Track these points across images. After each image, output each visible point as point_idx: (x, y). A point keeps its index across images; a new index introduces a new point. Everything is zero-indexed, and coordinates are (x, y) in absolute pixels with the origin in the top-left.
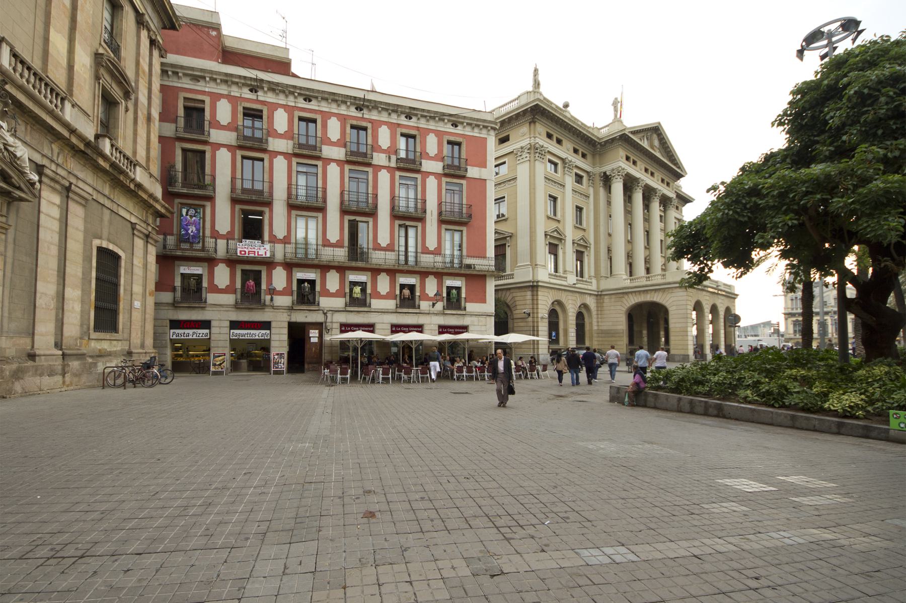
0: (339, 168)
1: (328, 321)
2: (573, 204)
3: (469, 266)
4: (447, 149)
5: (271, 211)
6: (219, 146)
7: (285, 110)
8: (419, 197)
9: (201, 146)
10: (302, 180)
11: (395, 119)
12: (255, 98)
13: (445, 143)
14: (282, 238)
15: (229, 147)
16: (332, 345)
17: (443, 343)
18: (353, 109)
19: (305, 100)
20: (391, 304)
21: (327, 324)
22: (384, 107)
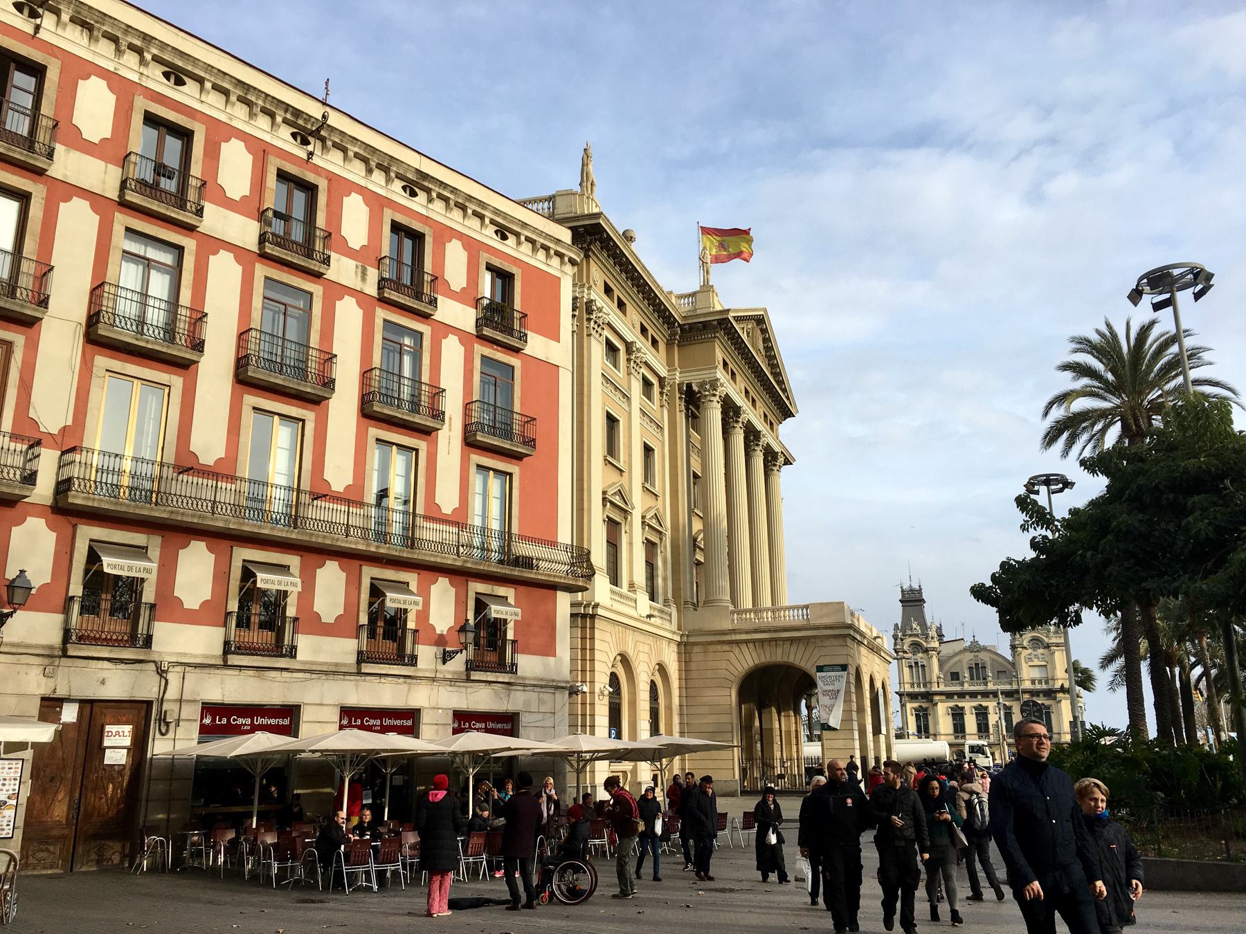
0: (240, 268)
1: (167, 696)
2: (603, 409)
3: (527, 563)
4: (140, 139)
5: (32, 347)
6: (219, 244)
7: (109, 86)
8: (185, 297)
9: (398, 316)
10: (129, 276)
11: (382, 187)
12: (29, 29)
13: (137, 119)
14: (55, 431)
15: (238, 252)
16: (172, 767)
17: (252, 760)
18: (285, 132)
19: (167, 75)
20: (344, 649)
21: (165, 707)
22: (361, 152)
